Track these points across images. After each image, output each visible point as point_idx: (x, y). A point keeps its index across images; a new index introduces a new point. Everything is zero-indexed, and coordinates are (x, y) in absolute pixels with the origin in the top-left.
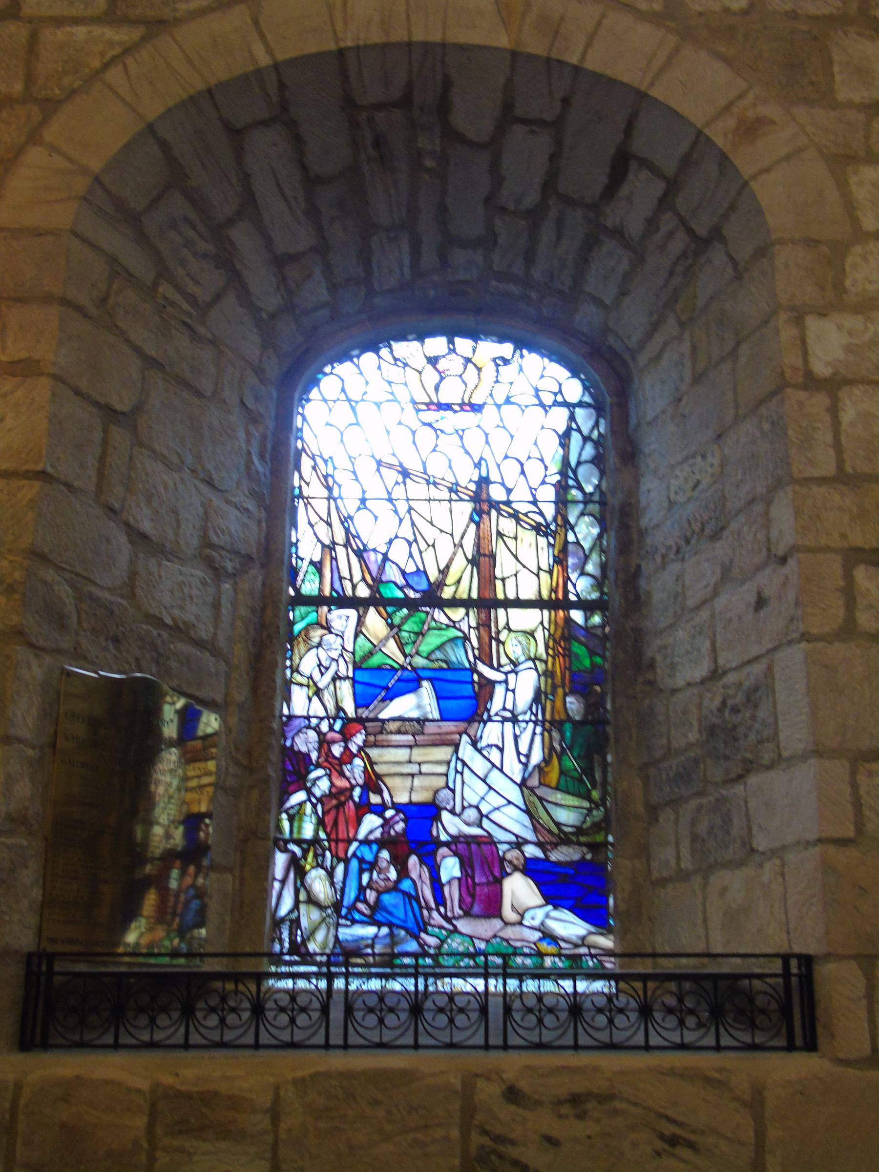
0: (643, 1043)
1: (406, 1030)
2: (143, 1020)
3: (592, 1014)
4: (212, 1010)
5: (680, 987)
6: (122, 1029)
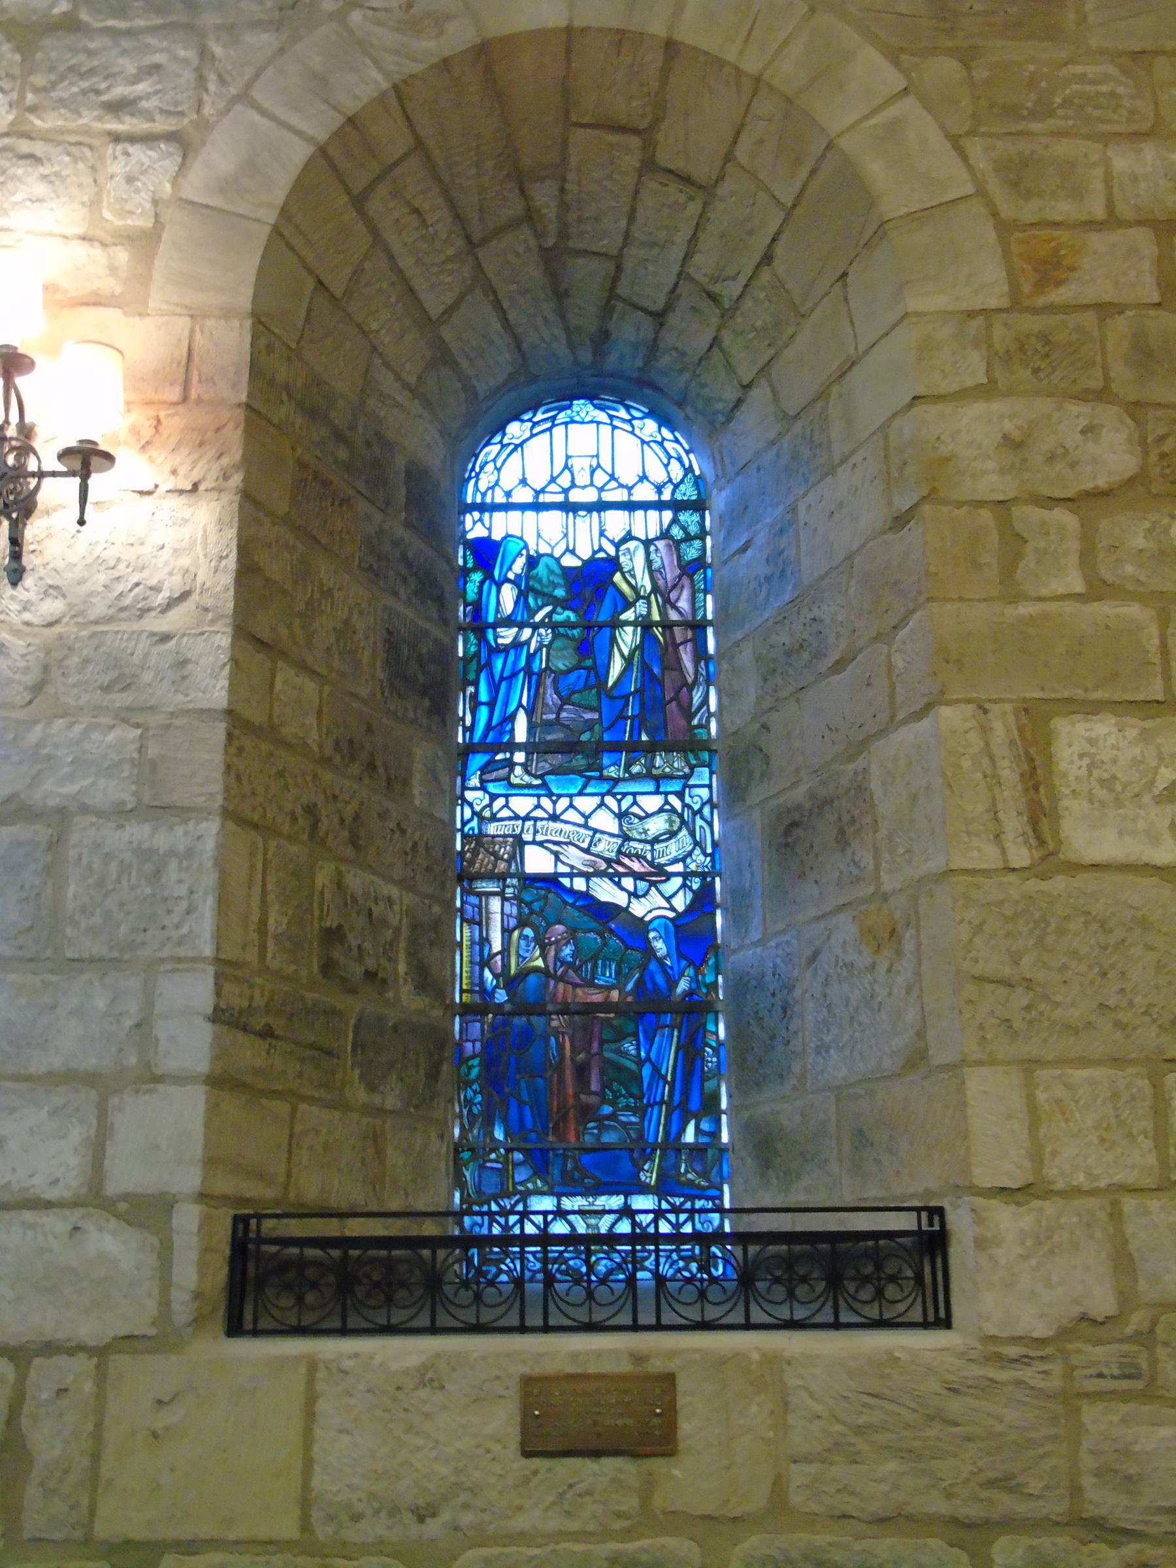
0: (921, 1320)
1: (510, 1308)
2: (866, 1294)
3: (566, 1286)
4: (866, 1280)
5: (545, 1252)
6: (440, 1310)
